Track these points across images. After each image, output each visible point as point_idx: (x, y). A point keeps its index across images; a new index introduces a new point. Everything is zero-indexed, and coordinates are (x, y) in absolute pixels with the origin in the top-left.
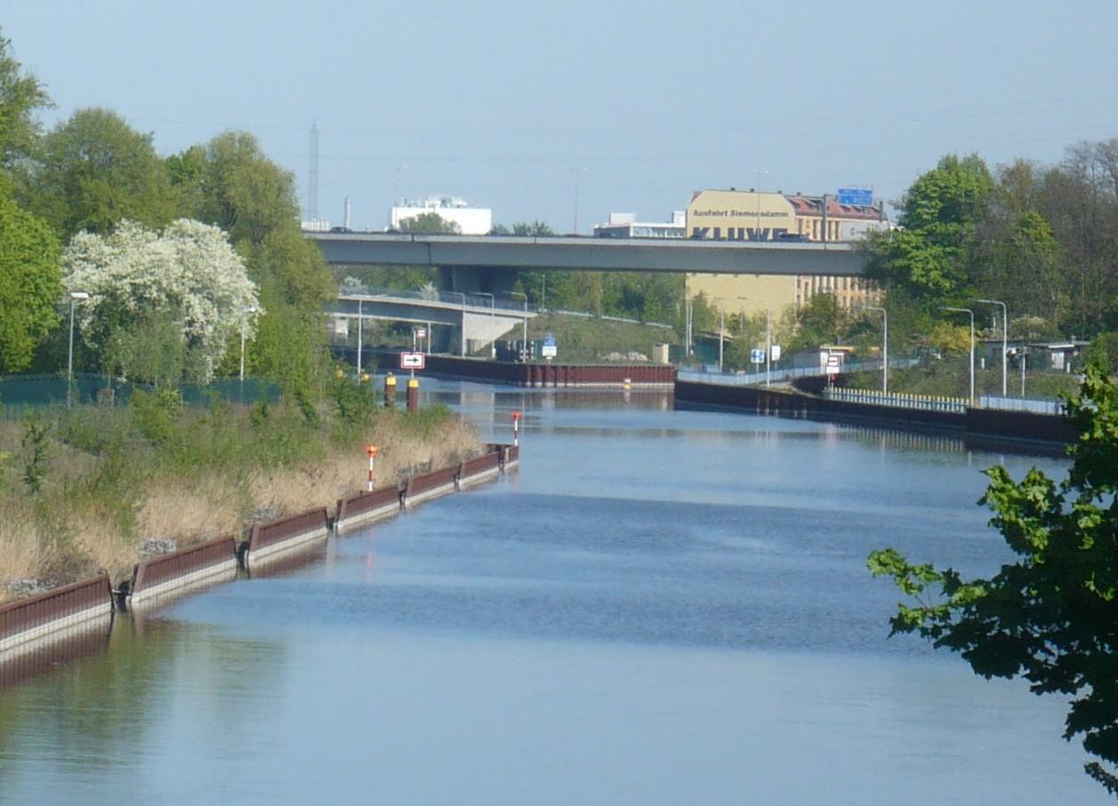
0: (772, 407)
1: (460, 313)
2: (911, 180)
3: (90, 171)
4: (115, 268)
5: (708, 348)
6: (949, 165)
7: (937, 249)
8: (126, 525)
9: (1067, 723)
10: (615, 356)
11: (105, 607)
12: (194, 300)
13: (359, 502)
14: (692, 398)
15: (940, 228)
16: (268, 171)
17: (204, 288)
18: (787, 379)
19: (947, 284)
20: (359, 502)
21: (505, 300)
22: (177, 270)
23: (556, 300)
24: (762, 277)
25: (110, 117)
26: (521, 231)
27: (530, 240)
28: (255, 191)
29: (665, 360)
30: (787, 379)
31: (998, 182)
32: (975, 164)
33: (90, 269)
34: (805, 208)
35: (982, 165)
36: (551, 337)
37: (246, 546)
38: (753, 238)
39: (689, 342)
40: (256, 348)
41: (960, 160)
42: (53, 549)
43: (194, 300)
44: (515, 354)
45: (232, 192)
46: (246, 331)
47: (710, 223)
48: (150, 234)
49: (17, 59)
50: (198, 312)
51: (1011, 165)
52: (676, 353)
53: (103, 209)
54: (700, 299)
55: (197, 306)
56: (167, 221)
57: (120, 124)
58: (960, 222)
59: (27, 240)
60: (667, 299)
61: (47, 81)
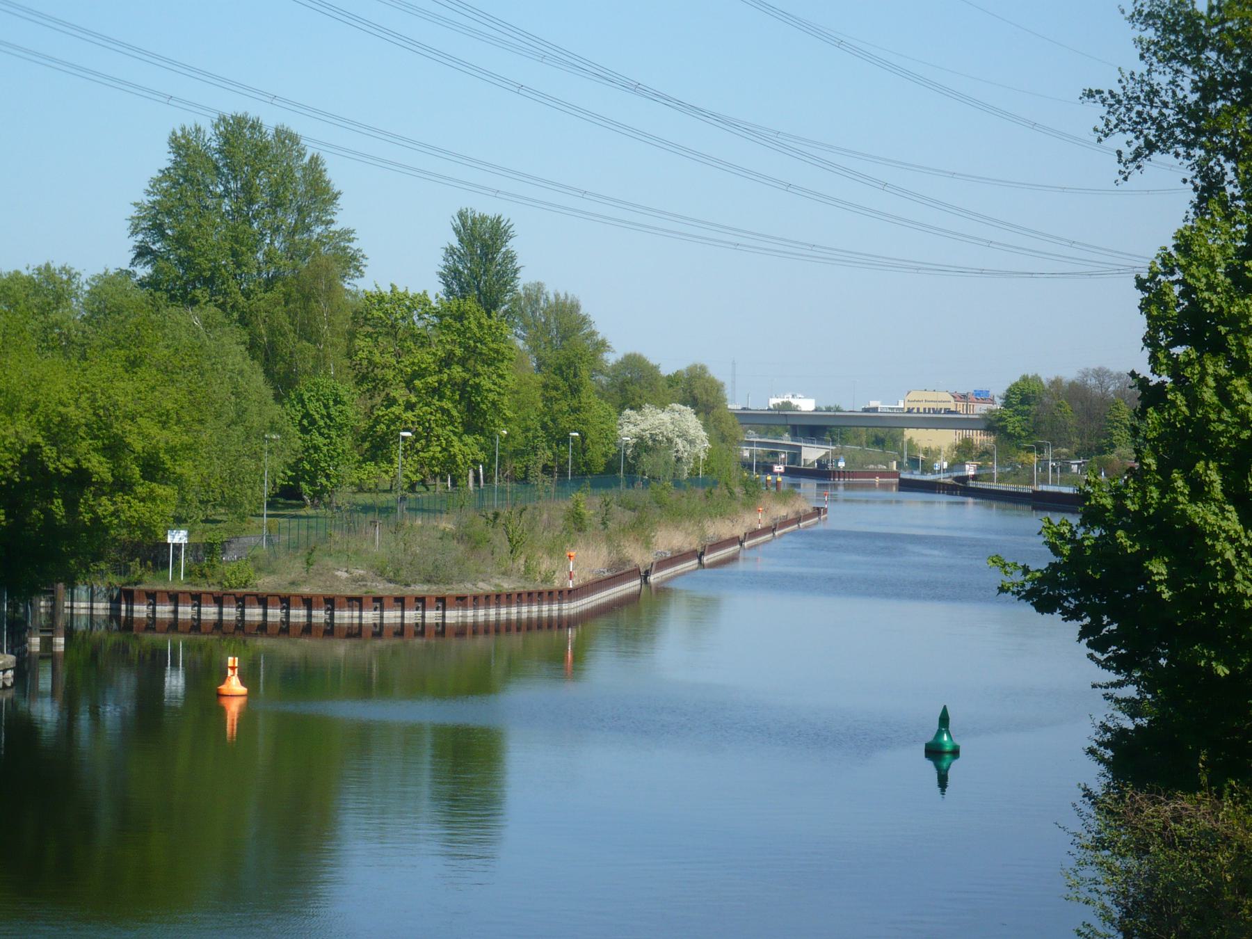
1: (800, 447)
2: (1007, 386)
3: (631, 382)
4: (643, 426)
5: (914, 462)
6: (1025, 379)
7: (1019, 418)
8: (647, 544)
10: (871, 466)
11: (638, 582)
12: (679, 441)
15: (1020, 408)
16: (712, 382)
17: (683, 435)
18: (950, 477)
20: (754, 533)
21: (821, 441)
23: (845, 441)
25: (635, 355)
26: (829, 409)
27: (832, 413)
30: (950, 477)
31: (1047, 387)
32: (1036, 379)
33: (631, 426)
34: (958, 399)
35: (1040, 379)
37: (702, 554)
40: (707, 463)
43: (679, 441)
46: (702, 455)
47: (915, 405)
48: (659, 411)
49: (598, 330)
50: (680, 446)
52: (900, 465)
53: (637, 399)
54: (910, 441)
55: (680, 444)
56: (667, 405)
60: (895, 441)
61: (612, 341)
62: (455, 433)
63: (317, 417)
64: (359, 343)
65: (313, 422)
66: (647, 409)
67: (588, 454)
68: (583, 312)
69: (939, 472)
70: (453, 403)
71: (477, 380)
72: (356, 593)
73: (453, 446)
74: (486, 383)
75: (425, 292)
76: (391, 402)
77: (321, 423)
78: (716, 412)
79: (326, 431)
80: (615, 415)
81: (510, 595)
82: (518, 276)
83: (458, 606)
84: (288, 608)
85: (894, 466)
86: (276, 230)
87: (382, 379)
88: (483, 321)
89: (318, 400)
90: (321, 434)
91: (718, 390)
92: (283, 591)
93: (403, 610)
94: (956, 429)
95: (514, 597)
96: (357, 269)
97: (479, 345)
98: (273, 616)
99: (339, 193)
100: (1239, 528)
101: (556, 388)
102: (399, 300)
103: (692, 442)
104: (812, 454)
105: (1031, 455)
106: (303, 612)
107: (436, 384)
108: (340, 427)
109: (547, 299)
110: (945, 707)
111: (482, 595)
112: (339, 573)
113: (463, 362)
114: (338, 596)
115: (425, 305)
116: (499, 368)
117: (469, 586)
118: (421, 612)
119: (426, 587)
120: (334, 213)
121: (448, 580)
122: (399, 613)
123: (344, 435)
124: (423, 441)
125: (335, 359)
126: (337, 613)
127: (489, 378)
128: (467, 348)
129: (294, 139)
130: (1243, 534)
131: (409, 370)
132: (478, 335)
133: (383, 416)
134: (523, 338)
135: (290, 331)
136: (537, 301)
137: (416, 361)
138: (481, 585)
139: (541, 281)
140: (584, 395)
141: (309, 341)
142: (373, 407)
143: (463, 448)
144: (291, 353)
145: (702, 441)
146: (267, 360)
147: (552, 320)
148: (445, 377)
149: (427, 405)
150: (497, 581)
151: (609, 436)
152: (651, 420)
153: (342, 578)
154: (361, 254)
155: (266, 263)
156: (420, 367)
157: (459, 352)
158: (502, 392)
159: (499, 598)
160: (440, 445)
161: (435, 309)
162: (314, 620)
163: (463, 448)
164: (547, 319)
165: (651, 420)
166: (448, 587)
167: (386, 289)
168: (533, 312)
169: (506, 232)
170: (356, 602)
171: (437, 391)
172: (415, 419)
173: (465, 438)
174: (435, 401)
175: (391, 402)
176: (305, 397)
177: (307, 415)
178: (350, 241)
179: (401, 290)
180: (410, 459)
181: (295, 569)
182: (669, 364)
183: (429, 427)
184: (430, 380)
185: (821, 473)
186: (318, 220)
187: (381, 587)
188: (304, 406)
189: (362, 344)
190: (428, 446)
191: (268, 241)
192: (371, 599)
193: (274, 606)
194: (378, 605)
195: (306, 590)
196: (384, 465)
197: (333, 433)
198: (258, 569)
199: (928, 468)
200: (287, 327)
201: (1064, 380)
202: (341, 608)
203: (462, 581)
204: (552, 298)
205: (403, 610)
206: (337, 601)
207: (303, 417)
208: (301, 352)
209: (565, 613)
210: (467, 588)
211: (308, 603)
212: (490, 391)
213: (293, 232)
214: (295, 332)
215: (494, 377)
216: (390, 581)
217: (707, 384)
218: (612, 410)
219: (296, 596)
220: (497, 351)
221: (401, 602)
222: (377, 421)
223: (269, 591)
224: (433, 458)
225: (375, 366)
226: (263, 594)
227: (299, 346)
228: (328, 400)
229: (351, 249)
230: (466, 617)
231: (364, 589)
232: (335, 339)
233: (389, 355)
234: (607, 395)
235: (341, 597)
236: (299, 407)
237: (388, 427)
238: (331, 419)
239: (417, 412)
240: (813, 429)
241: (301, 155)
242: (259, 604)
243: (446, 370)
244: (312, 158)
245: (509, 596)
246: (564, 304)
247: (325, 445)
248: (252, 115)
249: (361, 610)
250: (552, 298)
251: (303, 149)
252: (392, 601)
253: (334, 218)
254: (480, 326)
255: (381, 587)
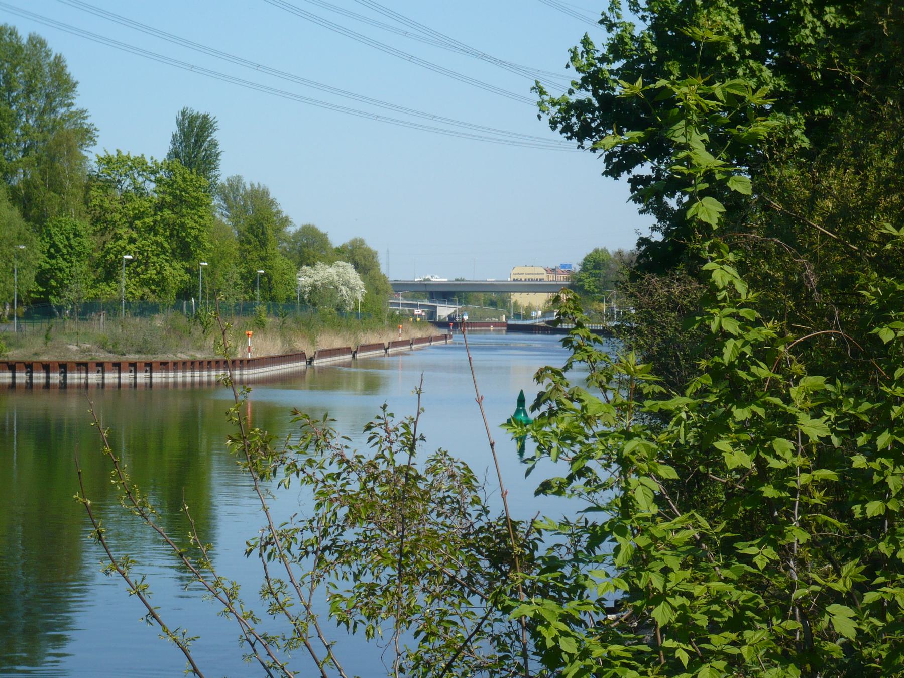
0: (539, 331)
1: (436, 307)
2: (584, 256)
3: (307, 245)
4: (316, 278)
5: (517, 316)
6: (596, 251)
7: (593, 279)
8: (313, 342)
9: (678, 658)
10: (487, 320)
11: (304, 363)
12: (343, 288)
13: (395, 344)
14: (512, 329)
15: (594, 272)
16: (369, 250)
17: (346, 284)
18: (543, 321)
19: (596, 290)
20: (395, 344)
21: (451, 302)
22: (336, 278)
23: (467, 303)
24: (537, 294)
25: (313, 227)
26: (457, 280)
27: (459, 282)
28: (364, 257)
29: (504, 320)
30: (543, 321)
31: (613, 256)
32: (605, 250)
33: (307, 278)
34: (549, 272)
35: (607, 251)
36: (466, 313)
37: (356, 352)
38: (535, 281)
39: (512, 314)
40: (363, 305)
41: (600, 249)
42: (287, 347)
43: (343, 288)
44: (454, 319)
45: (356, 258)
46: (360, 299)
47: (518, 277)
48: (327, 266)
49: (283, 210)
50: (344, 292)
51: (617, 250)
52: (507, 318)
53: (312, 258)
54: (515, 304)
55: (344, 289)
56: (333, 262)
57: (316, 229)
58: (600, 269)
59: (285, 267)
60: (504, 303)
61: (293, 218)
62: (167, 261)
63: (61, 246)
64: (93, 193)
65: (58, 250)
66: (319, 265)
67: (274, 291)
68: (271, 197)
69: (535, 319)
70: (164, 237)
71: (183, 220)
72: (84, 360)
73: (165, 270)
74: (189, 222)
75: (142, 155)
76: (117, 238)
77: (65, 251)
78: (372, 272)
79: (68, 257)
80: (295, 268)
81: (202, 362)
82: (219, 158)
83: (162, 369)
84: (31, 372)
85: (504, 319)
86: (30, 111)
87: (111, 221)
88: (186, 176)
89: (62, 234)
90: (65, 259)
91: (373, 257)
92: (26, 359)
93: (119, 372)
94: (548, 292)
95: (205, 364)
96: (91, 139)
97: (183, 194)
98: (20, 378)
99: (77, 83)
100: (740, 26)
101: (249, 243)
102: (123, 161)
103: (352, 289)
104: (444, 311)
105: (601, 304)
106: (43, 375)
107: (152, 224)
108: (79, 254)
109: (244, 187)
110: (522, 391)
111: (180, 362)
112: (71, 347)
113: (171, 207)
114: (69, 362)
115: (143, 164)
116: (199, 211)
117: (171, 355)
118: (133, 374)
119: (137, 356)
120: (73, 98)
121: (155, 352)
122: (116, 375)
123: (82, 260)
124: (143, 267)
125: (76, 204)
126: (69, 375)
127: (192, 218)
128: (175, 197)
129: (43, 44)
130: (743, 33)
131: (131, 213)
132: (183, 186)
133: (112, 248)
134: (227, 217)
135: (42, 185)
136: (237, 189)
137: (137, 206)
138: (179, 355)
139: (240, 175)
140: (269, 247)
141: (55, 192)
142: (105, 243)
143: (173, 272)
144: (42, 201)
145: (360, 288)
146: (25, 208)
147: (249, 203)
148: (158, 218)
149: (145, 239)
150: (193, 353)
151: (291, 284)
152: (322, 273)
153: (73, 350)
154: (94, 127)
155: (23, 135)
156: (139, 211)
157: (168, 199)
158: (202, 228)
159: (194, 365)
160: (156, 269)
161: (150, 168)
162: (51, 381)
163: (173, 272)
164: (245, 202)
165: (322, 273)
166: (154, 356)
167: (113, 153)
168: (235, 198)
169: (212, 125)
170: (83, 366)
171: (152, 229)
172: (136, 250)
173: (174, 264)
174: (151, 236)
175: (117, 238)
176: (52, 232)
177: (53, 245)
178: (84, 118)
179: (124, 153)
180: (133, 280)
181: (38, 344)
182: (337, 239)
183: (147, 256)
184: (147, 220)
185: (452, 324)
186: (61, 104)
187: (103, 355)
188: (51, 238)
189: (95, 194)
190: (147, 270)
191: (24, 119)
192: (95, 364)
193: (21, 371)
194: (100, 368)
195: (45, 358)
196: (113, 284)
197: (74, 259)
198: (9, 345)
199: (528, 317)
200: (39, 182)
201: (624, 252)
202: (72, 371)
203: (165, 352)
204: (248, 187)
205: (119, 372)
206: (69, 366)
207: (50, 247)
208: (49, 200)
209: (245, 377)
210: (169, 357)
211: (47, 368)
212: (193, 228)
213: (43, 113)
214: (45, 185)
215: (196, 217)
216: (110, 352)
217: (366, 253)
218: (292, 265)
219: (36, 362)
220: (198, 199)
221: (118, 367)
222: (108, 252)
223: (17, 359)
224: (150, 279)
225: (106, 211)
226: (11, 361)
227: (48, 195)
228: (69, 233)
229: (86, 124)
230: (169, 377)
231: (90, 357)
232: (74, 190)
233: (116, 203)
234: (289, 255)
235: (71, 362)
236: (47, 240)
237: (116, 256)
238: (72, 248)
239: (137, 244)
240: (445, 294)
241: (48, 55)
242: (9, 369)
243: (159, 213)
244: (56, 57)
245: (201, 363)
246: (257, 191)
247: (67, 267)
248: (10, 24)
249: (87, 372)
250: (248, 187)
251: (50, 51)
252: (111, 366)
253: (73, 101)
254: (184, 180)
255: (103, 355)
